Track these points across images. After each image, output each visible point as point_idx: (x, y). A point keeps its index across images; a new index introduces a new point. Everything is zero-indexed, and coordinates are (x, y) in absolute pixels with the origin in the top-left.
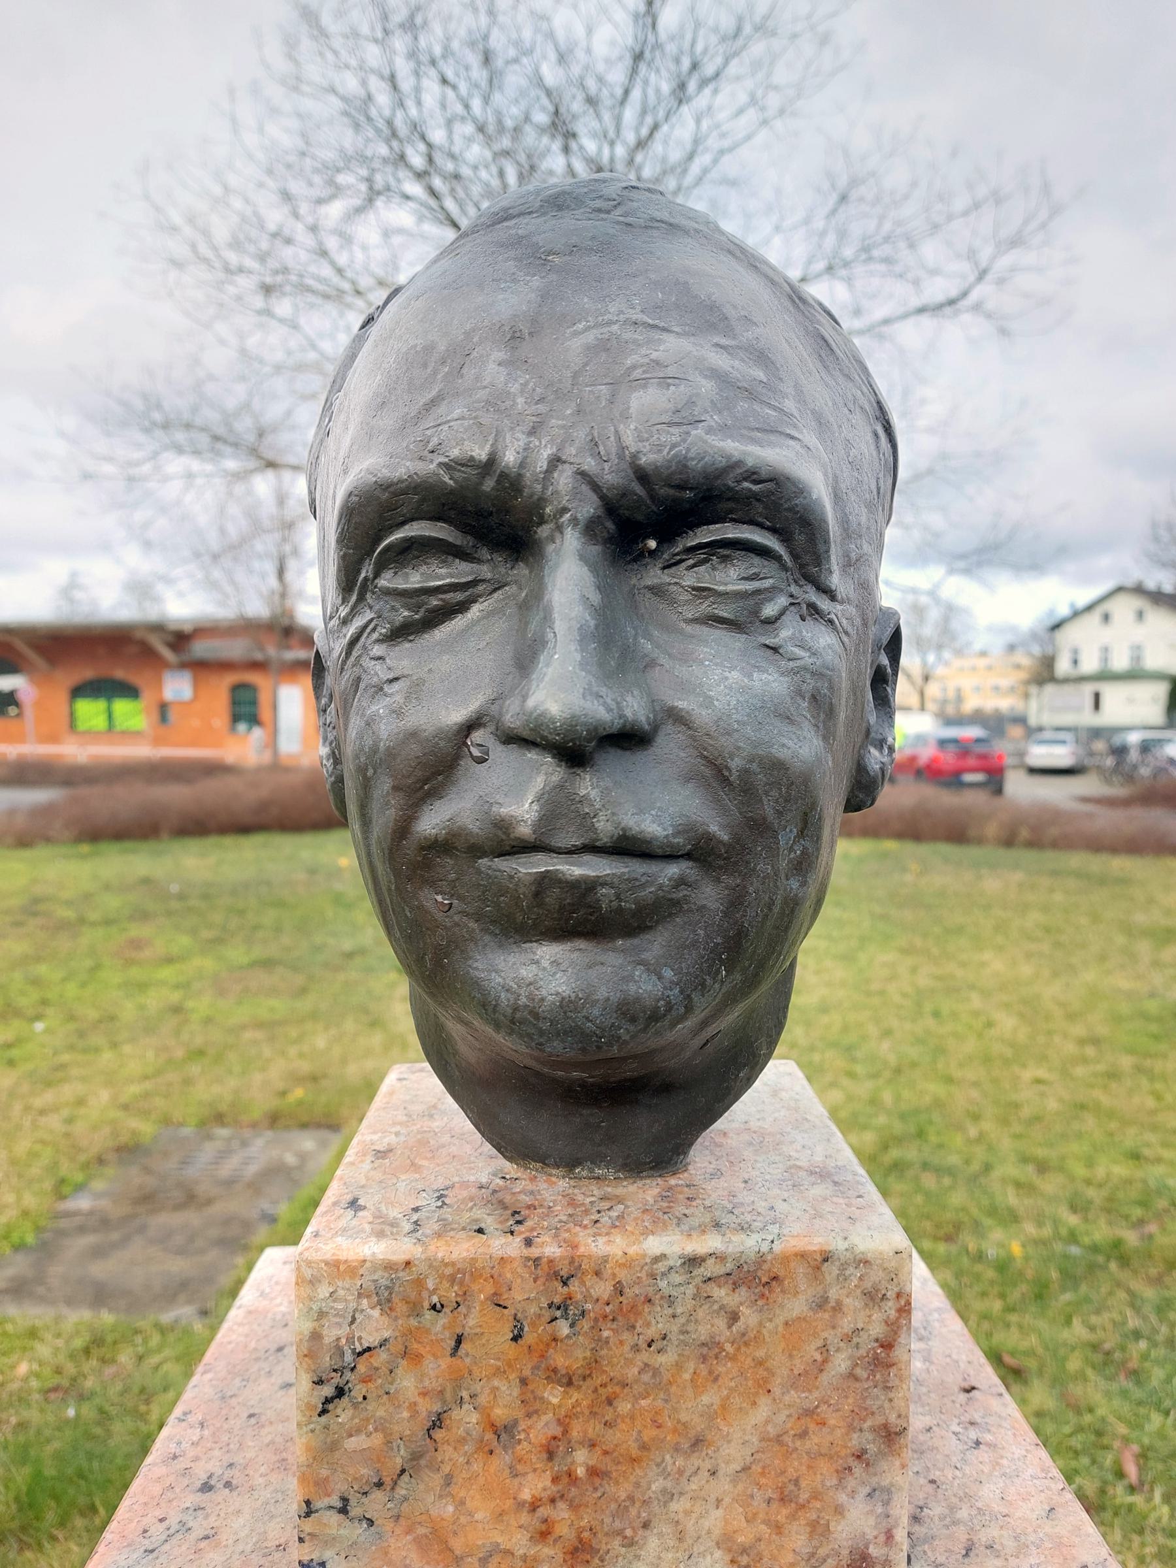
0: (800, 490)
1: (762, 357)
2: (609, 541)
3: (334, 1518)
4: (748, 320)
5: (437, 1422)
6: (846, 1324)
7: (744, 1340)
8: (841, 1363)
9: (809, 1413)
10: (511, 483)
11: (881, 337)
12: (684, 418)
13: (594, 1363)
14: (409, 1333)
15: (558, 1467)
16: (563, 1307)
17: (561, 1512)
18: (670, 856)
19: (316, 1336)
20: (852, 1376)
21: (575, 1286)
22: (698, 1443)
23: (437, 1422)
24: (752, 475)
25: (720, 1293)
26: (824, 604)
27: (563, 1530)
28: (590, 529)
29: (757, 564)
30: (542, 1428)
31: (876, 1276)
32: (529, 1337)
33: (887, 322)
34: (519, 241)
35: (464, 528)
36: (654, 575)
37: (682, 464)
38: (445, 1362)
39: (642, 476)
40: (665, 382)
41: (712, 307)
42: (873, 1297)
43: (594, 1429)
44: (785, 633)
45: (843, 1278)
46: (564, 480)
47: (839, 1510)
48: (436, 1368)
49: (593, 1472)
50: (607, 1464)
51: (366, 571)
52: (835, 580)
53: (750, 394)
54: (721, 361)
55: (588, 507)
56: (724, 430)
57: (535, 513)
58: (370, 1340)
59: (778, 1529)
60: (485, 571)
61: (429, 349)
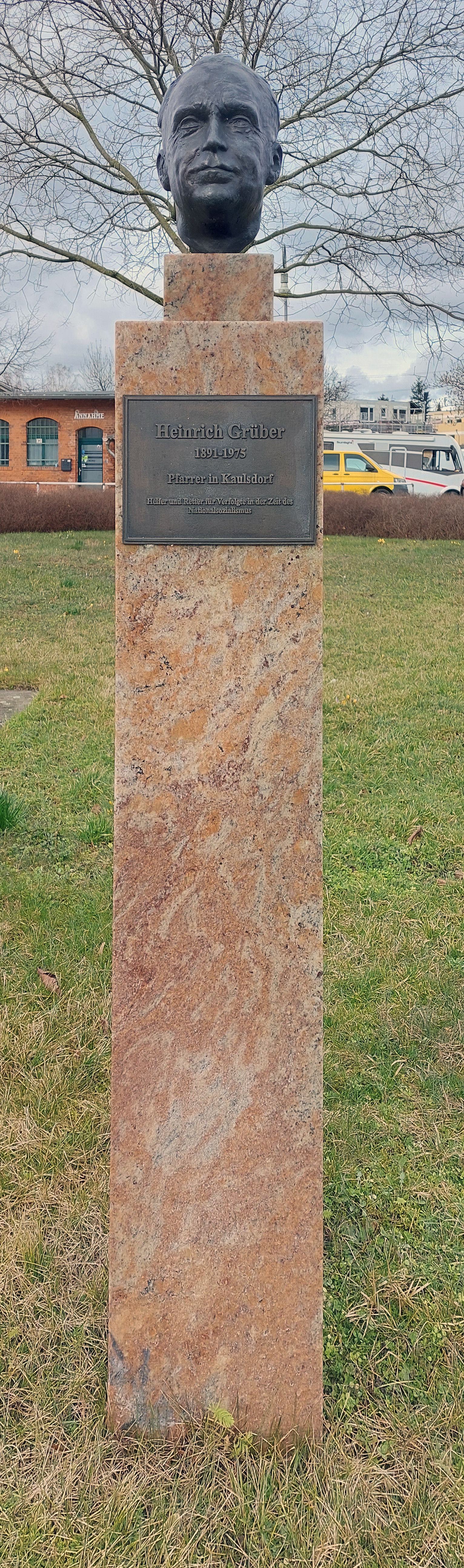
0: (252, 109)
1: (246, 87)
2: (220, 117)
3: (171, 306)
4: (244, 81)
5: (189, 287)
6: (262, 270)
7: (243, 272)
8: (261, 277)
9: (255, 287)
10: (205, 107)
11: (445, 108)
12: (232, 96)
13: (217, 277)
14: (184, 270)
15: (210, 297)
16: (211, 265)
17: (211, 306)
18: (229, 171)
19: (168, 270)
20: (263, 280)
21: (213, 261)
22: (235, 293)
23: (189, 287)
24: (243, 106)
25: (239, 263)
26: (257, 132)
27: (211, 310)
28: (217, 115)
29: (244, 122)
30: (207, 289)
31: (267, 260)
32: (205, 271)
33: (446, 95)
34: (205, 67)
35: (196, 117)
36: (228, 125)
37: (232, 104)
38: (191, 275)
39: (225, 106)
40: (229, 91)
41: (238, 78)
42: (266, 265)
43: (217, 289)
44: (250, 135)
45: (261, 261)
46: (213, 107)
47: (261, 307)
48: (189, 277)
49: (217, 298)
50: (218, 296)
51: (179, 126)
52: (260, 128)
53: (244, 93)
54: (238, 87)
55: (217, 111)
56: (239, 99)
57: (209, 113)
58: (178, 271)
59: (250, 311)
60: (199, 124)
61: (191, 86)
